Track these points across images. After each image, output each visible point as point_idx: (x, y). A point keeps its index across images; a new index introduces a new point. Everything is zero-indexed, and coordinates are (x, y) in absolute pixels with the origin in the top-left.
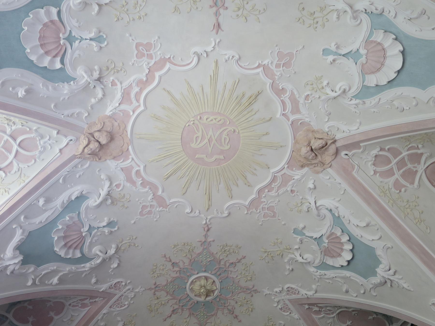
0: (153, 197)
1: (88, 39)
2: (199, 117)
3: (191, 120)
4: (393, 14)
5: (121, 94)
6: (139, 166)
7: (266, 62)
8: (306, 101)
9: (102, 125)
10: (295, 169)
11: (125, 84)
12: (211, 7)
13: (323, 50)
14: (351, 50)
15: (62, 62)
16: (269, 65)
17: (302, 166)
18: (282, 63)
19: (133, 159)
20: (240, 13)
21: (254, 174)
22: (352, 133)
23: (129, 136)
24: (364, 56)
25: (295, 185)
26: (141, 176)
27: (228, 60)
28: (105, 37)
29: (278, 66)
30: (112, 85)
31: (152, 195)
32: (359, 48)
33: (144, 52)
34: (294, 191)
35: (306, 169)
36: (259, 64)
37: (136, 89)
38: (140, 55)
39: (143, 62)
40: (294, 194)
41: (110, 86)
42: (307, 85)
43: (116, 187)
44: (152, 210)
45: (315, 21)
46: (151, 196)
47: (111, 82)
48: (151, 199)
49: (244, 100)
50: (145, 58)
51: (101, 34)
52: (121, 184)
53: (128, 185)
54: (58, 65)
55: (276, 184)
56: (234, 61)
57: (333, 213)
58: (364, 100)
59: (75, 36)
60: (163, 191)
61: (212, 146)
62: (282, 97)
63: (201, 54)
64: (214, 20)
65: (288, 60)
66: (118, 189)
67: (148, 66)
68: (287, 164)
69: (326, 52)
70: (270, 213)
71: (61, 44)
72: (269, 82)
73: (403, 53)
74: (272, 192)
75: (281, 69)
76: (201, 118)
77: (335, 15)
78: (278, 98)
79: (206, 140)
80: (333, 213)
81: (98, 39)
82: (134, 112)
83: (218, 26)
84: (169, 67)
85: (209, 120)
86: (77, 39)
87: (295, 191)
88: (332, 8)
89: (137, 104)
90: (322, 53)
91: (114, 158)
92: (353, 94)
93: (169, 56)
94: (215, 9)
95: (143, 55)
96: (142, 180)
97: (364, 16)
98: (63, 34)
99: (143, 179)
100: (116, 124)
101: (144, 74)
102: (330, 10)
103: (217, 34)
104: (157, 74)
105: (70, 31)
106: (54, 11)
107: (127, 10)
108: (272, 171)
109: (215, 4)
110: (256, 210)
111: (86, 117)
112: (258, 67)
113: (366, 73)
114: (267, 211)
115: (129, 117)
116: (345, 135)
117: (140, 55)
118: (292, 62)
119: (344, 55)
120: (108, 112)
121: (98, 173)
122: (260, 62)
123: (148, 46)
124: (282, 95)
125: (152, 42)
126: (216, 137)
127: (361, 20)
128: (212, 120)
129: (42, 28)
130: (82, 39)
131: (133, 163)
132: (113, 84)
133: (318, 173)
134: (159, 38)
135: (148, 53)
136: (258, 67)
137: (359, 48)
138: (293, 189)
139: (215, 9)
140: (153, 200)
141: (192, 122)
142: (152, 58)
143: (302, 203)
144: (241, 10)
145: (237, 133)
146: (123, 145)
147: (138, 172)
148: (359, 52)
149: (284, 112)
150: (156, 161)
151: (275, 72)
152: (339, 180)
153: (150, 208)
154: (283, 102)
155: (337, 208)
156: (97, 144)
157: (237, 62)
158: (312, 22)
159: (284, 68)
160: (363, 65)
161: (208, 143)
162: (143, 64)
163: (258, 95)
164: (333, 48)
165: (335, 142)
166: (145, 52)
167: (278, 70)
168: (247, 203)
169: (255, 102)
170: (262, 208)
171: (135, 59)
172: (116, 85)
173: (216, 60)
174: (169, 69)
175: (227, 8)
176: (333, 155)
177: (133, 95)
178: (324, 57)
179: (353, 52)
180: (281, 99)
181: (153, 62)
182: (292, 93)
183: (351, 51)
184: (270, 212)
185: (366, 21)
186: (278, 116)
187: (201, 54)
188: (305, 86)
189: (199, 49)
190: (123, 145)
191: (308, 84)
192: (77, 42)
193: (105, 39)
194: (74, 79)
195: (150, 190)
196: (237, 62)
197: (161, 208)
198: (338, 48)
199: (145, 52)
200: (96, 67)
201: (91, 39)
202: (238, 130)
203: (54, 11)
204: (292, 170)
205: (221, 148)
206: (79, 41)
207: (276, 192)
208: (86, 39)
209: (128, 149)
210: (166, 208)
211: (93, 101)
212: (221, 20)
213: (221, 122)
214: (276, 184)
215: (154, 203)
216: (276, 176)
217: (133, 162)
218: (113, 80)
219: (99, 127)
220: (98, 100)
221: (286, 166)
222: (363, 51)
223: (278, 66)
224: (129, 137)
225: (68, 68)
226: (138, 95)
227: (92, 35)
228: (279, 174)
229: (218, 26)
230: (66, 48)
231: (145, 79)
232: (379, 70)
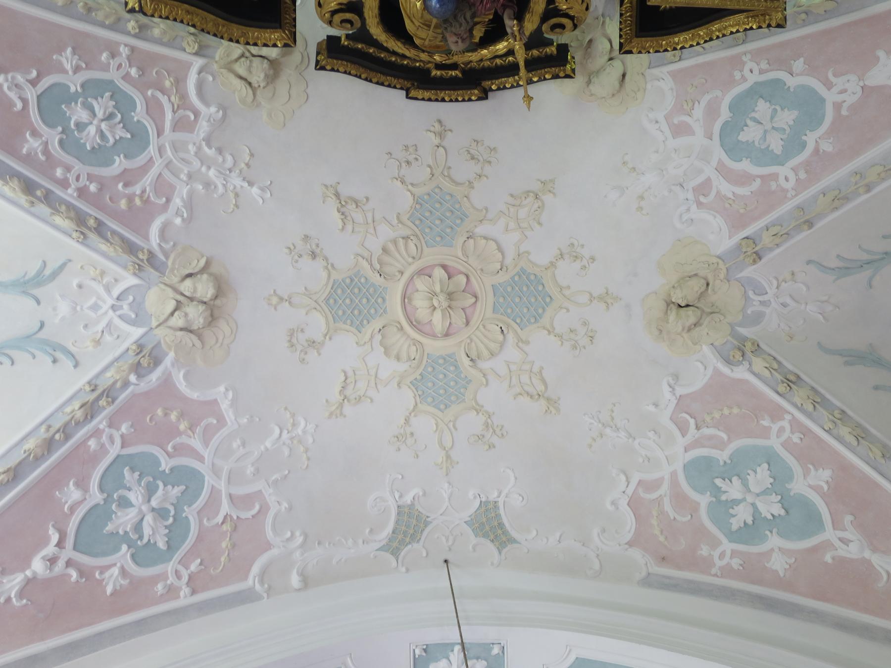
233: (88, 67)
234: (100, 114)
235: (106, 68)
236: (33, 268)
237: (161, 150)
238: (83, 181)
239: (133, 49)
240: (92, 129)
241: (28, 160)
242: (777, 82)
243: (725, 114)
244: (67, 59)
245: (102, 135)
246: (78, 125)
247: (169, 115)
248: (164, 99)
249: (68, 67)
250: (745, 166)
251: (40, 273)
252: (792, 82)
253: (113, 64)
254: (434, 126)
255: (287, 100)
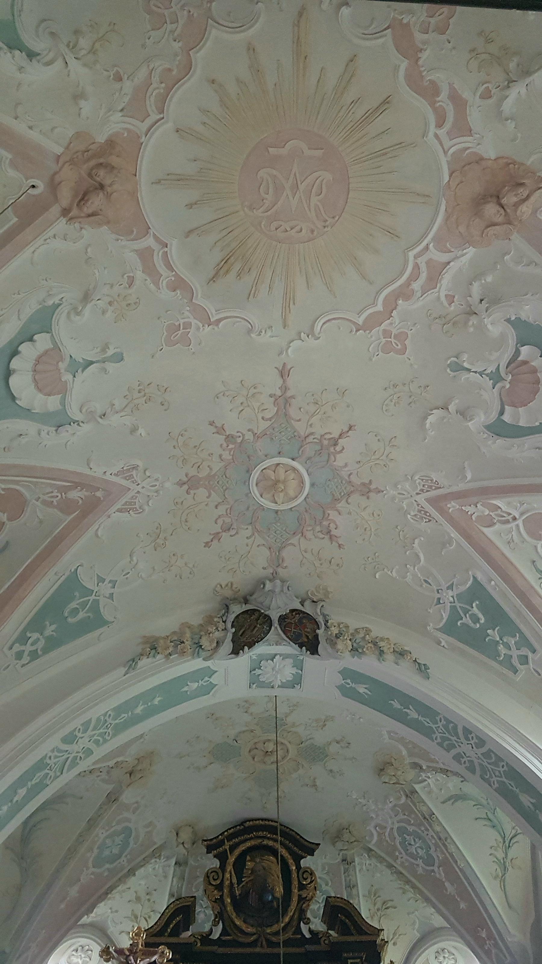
0: (420, 55)
1: (473, 372)
2: (315, 233)
3: (329, 228)
4: (43, 434)
5: (442, 282)
6: (436, 136)
7: (208, 329)
8: (132, 275)
9: (485, 231)
10: (123, 134)
11: (431, 296)
12: (293, 397)
13: (122, 359)
14: (84, 372)
15: (517, 353)
16: (202, 325)
17: (111, 143)
18: (182, 331)
19: (445, 153)
20: (253, 391)
21: (205, 111)
22: (40, 241)
23: (444, 202)
24: (62, 371)
25: (117, 94)
26: (435, 110)
27: (267, 329)
28: (448, 370)
29: (187, 326)
30: (454, 297)
31: (420, 62)
32: (74, 380)
33: (395, 341)
34: (115, 80)
35: (101, 139)
36: (217, 325)
37: (416, 286)
38: (401, 337)
39: (398, 327)
40: (113, 72)
41: (456, 297)
42: (137, 302)
43: (492, 92)
44: (427, 16)
45: (143, 393)
46: (424, 56)
47: (453, 302)
48: (426, 50)
49: (237, 267)
50: (394, 332)
51: (452, 374)
52: (480, 98)
53: (466, 95)
54: (525, 350)
55: (157, 91)
56: (257, 328)
57: (24, 53)
58: (41, 306)
59: (490, 380)
60: (396, 68)
61: (292, 176)
62: (173, 276)
63: (308, 337)
64: (290, 381)
65: (173, 335)
66: (488, 87)
67: (392, 320)
68: (142, 144)
69: (119, 358)
70: (159, 7)
71: (511, 376)
72: (199, 300)
73: (13, 398)
74: (161, 68)
75: (182, 321)
76: (312, 231)
77: (117, 407)
78: (179, 273)
79: (302, 187)
80: (24, 53)
81: (458, 368)
82: (427, 248)
83: (284, 373)
84: (359, 317)
85: (298, 228)
86: (487, 375)
87: (113, 79)
88: (123, 414)
89: (419, 260)
90: (124, 355)
91: (480, 160)
92: (62, 311)
93: (358, 333)
94: (289, 394)
95: (396, 337)
96: (435, 102)
97: (78, 417)
98: (504, 387)
99: (432, 104)
100: (462, 229)
101: (399, 308)
102: (125, 410)
103: (285, 363)
104: (380, 307)
105: (494, 388)
106: (506, 418)
107: (410, 397)
108: (168, 126)
109: (287, 401)
110: (191, 13)
111: (507, 253)
112: (219, 321)
113: (52, 350)
114: (166, 12)
115: (437, 240)
116: (50, 233)
117: (401, 337)
118: (165, 334)
119: (92, 363)
120: (471, 251)
121: (519, 135)
122: (216, 328)
123: (387, 349)
124: (173, 279)
125: (381, 353)
126: (285, 194)
127: (81, 412)
128: (291, 229)
129: (529, 403)
130: (481, 374)
131: (447, 143)
132: (451, 299)
133: (78, 135)
134: (371, 360)
135: (390, 339)
136: (219, 321)
137: (74, 380)
138: (118, 85)
139: (289, 394)
140: (421, 46)
141: (328, 223)
142: (384, 331)
143: (92, 51)
144: (250, 395)
145: (246, 203)
146: (458, 185)
147: (440, 125)
148: (71, 373)
149: (166, 249)
150: (403, 145)
151: (190, 315)
152: (34, 135)
153: (430, 23)
154: (170, 267)
155: (21, 69)
156: (504, 201)
157: (252, 326)
158: (146, 391)
159: (177, 324)
160: (62, 359)
161: (299, 183)
162: (399, 323)
163: (213, 278)
164: (111, 367)
165: (65, 212)
166: (393, 340)
167: (186, 320)
168: (214, 33)
169: (218, 265)
170: (178, 21)
171: (409, 333)
172: (446, 296)
173: (286, 328)
174: (360, 313)
175: (271, 396)
176: (61, 182)
177: (424, 276)
178: (118, 350)
179: (80, 371)
180: (174, 273)
181: (383, 326)
182: (156, 284)
183: (83, 371)
184: (159, 10)
185: (74, 413)
186: (175, 242)
187: (308, 337)
188: (138, 300)
189: (311, 342)
190: (458, 185)
191: (135, 303)
192: (488, 371)
193: (449, 366)
194: (508, 320)
195: (424, 74)
196: (252, 326)
197: (405, 21)
198: (105, 370)
199: (393, 340)
200: (472, 330)
201: (469, 370)
202: (244, 210)
203: (506, 418)
204: (129, 131)
205: (275, 172)
206: (486, 372)
207: (153, 72)
208: (476, 372)
209: (451, 176)
210: (394, 19)
211: (489, 279)
212: (280, 382)
213: (275, 224)
214: (157, 91)
215: (419, 37)
216: (160, 113)
217: (446, 148)
218: (450, 305)
219: (492, 231)
220: (481, 280)
221: (143, 139)
222: (68, 377)
223: (187, 326)
224: (444, 200)
225: (512, 341)
226: (414, 277)
227: (465, 376)
228: (155, 117)
229: (284, 373)
230: (507, 368)
231: (400, 302)
232: (38, 361)
233: (414, 864)
234: (414, 848)
235: (406, 860)
236: (459, 803)
237: (393, 823)
238: (426, 832)
239: (395, 861)
240: (418, 845)
241: (443, 853)
242: (112, 863)
243: (132, 841)
244: (420, 871)
245: (414, 840)
246: (422, 849)
247: (387, 834)
248: (388, 839)
249: (420, 868)
250: (119, 828)
251: (456, 801)
252: (107, 866)
253: (403, 860)
254: (182, 502)
255: (292, 370)
